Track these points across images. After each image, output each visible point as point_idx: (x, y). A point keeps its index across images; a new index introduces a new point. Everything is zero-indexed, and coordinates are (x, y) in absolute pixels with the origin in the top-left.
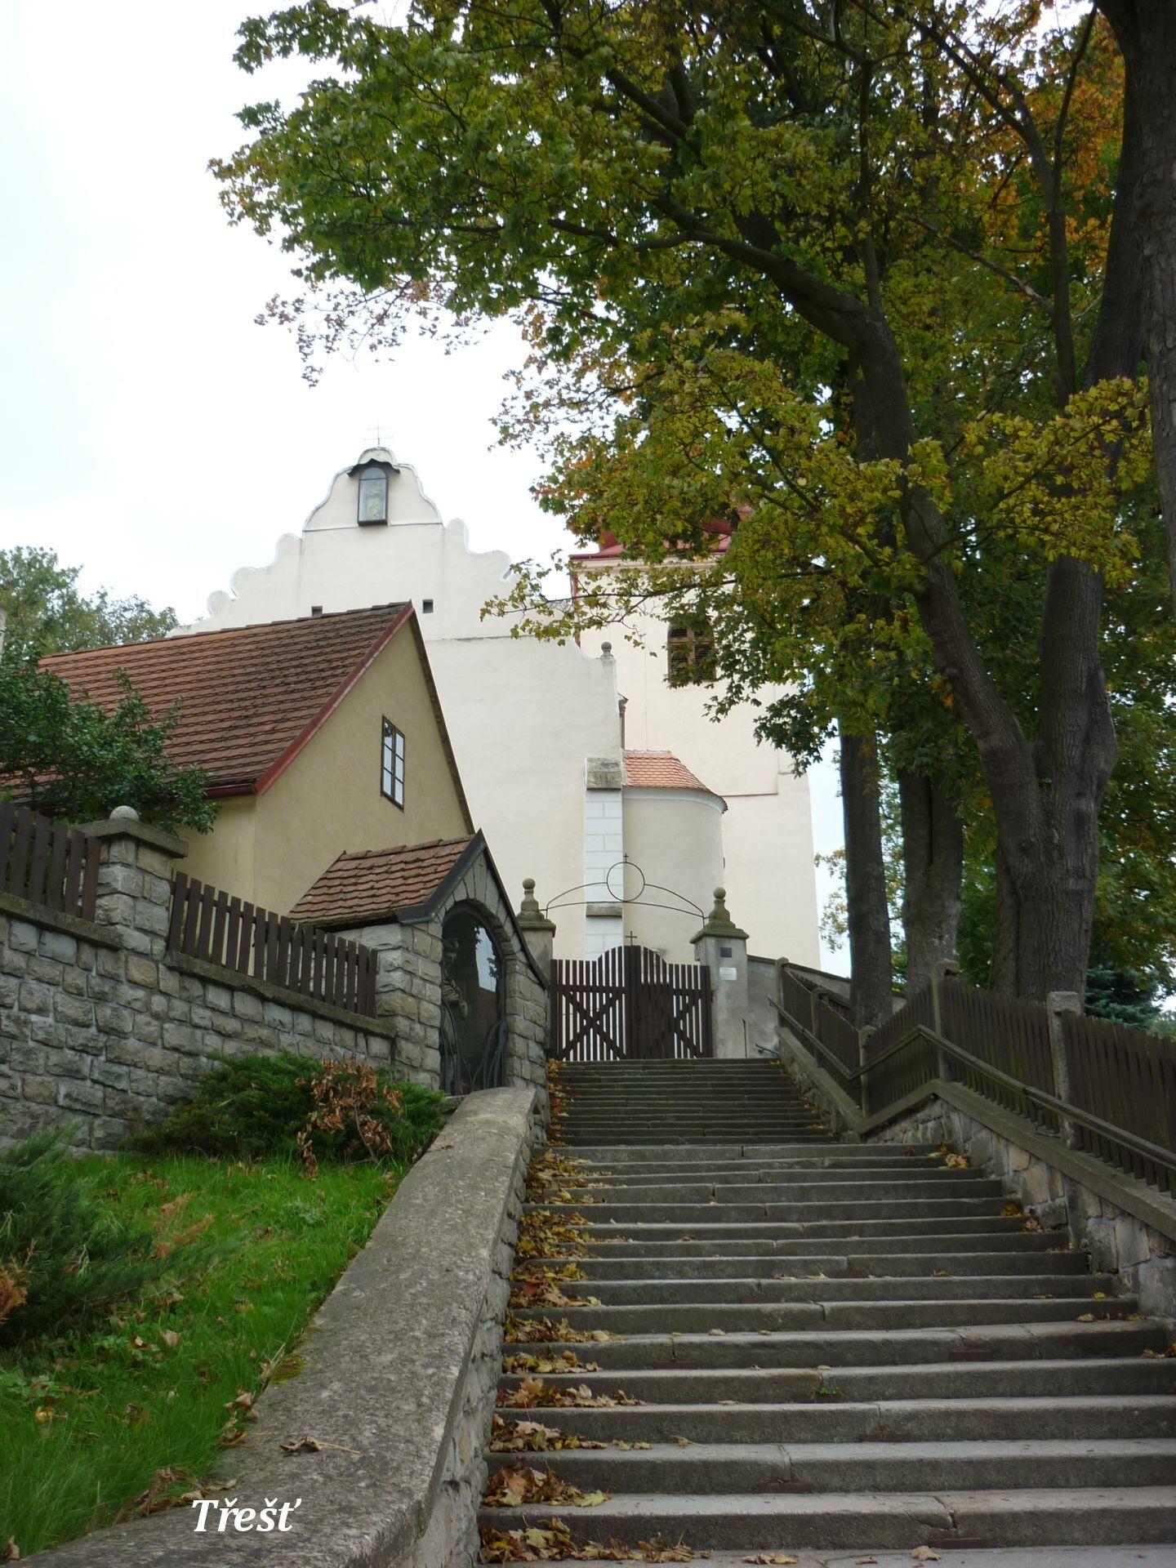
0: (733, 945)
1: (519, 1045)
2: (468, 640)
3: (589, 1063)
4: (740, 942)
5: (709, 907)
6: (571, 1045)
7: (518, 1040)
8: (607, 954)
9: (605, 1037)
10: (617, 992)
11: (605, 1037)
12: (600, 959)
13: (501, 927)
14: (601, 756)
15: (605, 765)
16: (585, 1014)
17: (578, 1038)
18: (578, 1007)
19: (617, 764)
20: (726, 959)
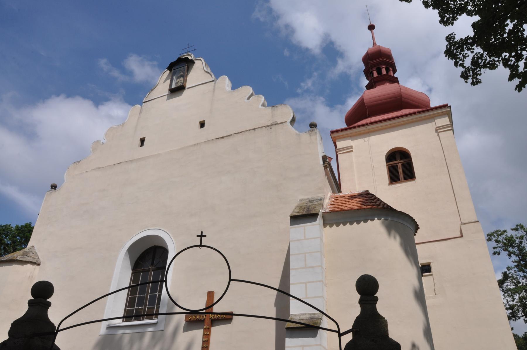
14: (310, 197)
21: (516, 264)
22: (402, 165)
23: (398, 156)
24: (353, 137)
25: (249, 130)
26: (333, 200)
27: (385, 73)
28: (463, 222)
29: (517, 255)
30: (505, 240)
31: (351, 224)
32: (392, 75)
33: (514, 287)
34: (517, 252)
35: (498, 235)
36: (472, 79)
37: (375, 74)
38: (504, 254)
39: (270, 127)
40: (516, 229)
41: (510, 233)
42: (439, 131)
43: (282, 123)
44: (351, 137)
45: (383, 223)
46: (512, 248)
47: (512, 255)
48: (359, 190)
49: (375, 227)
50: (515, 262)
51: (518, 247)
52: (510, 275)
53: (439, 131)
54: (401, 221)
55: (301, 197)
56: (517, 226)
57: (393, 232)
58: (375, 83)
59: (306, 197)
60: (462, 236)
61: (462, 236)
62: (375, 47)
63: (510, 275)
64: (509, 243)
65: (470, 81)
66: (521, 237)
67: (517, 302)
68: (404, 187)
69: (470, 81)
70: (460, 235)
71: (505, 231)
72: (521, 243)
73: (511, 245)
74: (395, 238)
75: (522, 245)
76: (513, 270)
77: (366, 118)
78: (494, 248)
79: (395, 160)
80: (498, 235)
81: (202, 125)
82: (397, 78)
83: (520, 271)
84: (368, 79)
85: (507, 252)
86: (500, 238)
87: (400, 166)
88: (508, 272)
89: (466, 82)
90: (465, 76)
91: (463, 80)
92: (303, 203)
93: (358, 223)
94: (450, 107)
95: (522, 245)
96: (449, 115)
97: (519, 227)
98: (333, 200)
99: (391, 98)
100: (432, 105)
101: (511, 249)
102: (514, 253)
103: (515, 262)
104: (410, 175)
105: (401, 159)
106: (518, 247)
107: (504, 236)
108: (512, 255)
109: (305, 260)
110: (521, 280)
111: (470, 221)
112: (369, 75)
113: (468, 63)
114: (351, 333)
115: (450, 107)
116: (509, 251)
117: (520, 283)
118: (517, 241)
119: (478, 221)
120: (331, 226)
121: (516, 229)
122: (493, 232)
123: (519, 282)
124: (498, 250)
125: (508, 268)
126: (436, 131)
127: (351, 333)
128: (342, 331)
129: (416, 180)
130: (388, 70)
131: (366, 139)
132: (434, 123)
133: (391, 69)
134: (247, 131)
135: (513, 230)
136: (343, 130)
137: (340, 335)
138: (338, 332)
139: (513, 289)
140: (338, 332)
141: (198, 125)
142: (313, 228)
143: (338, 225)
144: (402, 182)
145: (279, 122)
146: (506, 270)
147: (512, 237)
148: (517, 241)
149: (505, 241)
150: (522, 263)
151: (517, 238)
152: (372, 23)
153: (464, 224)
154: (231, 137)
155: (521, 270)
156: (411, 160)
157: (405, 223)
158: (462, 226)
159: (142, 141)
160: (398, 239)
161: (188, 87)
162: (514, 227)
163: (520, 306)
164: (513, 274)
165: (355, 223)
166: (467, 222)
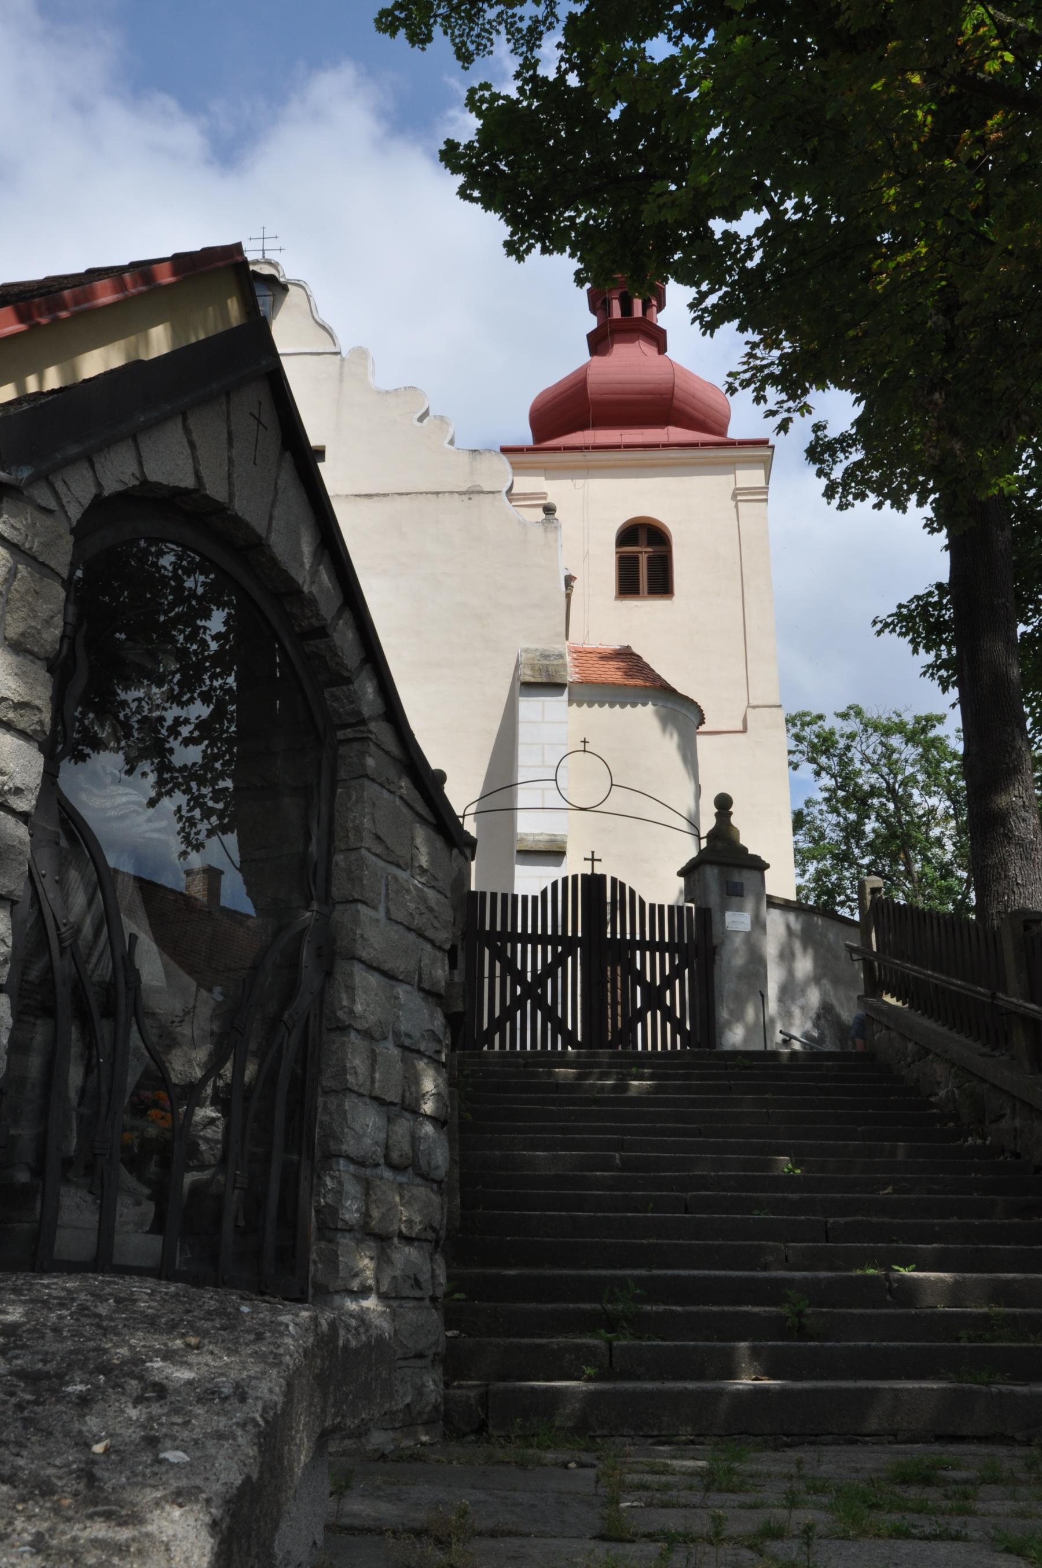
0: (746, 877)
1: (364, 998)
2: (369, 496)
3: (513, 1053)
4: (756, 874)
5: (708, 823)
6: (497, 1025)
7: (366, 981)
8: (555, 885)
9: (550, 1014)
10: (570, 944)
11: (550, 1014)
12: (544, 893)
13: (322, 632)
14: (540, 646)
15: (546, 656)
16: (519, 977)
17: (508, 1013)
18: (509, 965)
19: (561, 656)
20: (735, 900)
21: (826, 795)
22: (649, 559)
23: (643, 536)
24: (551, 472)
25: (427, 493)
26: (575, 655)
28: (753, 702)
29: (833, 776)
30: (817, 736)
31: (612, 706)
33: (811, 845)
34: (836, 769)
35: (804, 725)
36: (841, 498)
37: (617, 313)
38: (807, 769)
40: (844, 716)
41: (831, 723)
42: (739, 498)
43: (493, 493)
44: (545, 469)
45: (657, 713)
46: (828, 758)
47: (823, 774)
48: (615, 643)
49: (644, 716)
50: (827, 790)
51: (840, 756)
52: (808, 818)
53: (739, 498)
54: (684, 711)
55: (525, 645)
56: (850, 708)
57: (670, 727)
59: (533, 646)
60: (745, 730)
61: (745, 730)
63: (808, 818)
64: (824, 744)
65: (836, 502)
66: (852, 736)
67: (808, 881)
68: (646, 610)
69: (836, 502)
70: (740, 728)
71: (821, 717)
72: (848, 748)
73: (826, 752)
74: (671, 735)
75: (849, 755)
76: (818, 807)
77: (583, 426)
78: (790, 752)
79: (635, 543)
80: (803, 725)
83: (831, 812)
85: (815, 766)
86: (807, 732)
87: (645, 560)
88: (805, 812)
89: (829, 503)
90: (829, 493)
91: (825, 500)
92: (533, 659)
93: (623, 705)
94: (773, 447)
95: (849, 755)
96: (767, 464)
97: (852, 712)
99: (650, 393)
100: (734, 432)
101: (823, 760)
102: (827, 769)
103: (827, 790)
104: (662, 584)
105: (649, 544)
106: (840, 756)
107: (815, 728)
108: (823, 774)
109: (543, 754)
110: (829, 833)
111: (766, 704)
112: (599, 304)
113: (837, 474)
115: (773, 447)
116: (818, 764)
117: (825, 838)
118: (842, 743)
119: (780, 706)
120: (580, 705)
121: (844, 716)
122: (793, 714)
123: (822, 836)
124: (795, 758)
125: (809, 803)
126: (734, 496)
129: (674, 598)
131: (580, 482)
132: (732, 476)
133: (654, 302)
134: (421, 493)
135: (838, 715)
136: (530, 450)
139: (809, 850)
142: (556, 705)
143: (590, 705)
144: (644, 598)
145: (486, 489)
146: (803, 806)
147: (832, 733)
148: (842, 743)
149: (816, 741)
150: (841, 794)
151: (842, 736)
153: (754, 707)
155: (835, 810)
156: (670, 551)
157: (689, 715)
158: (750, 711)
160: (676, 737)
162: (843, 709)
163: (814, 889)
164: (814, 818)
165: (618, 706)
166: (760, 704)
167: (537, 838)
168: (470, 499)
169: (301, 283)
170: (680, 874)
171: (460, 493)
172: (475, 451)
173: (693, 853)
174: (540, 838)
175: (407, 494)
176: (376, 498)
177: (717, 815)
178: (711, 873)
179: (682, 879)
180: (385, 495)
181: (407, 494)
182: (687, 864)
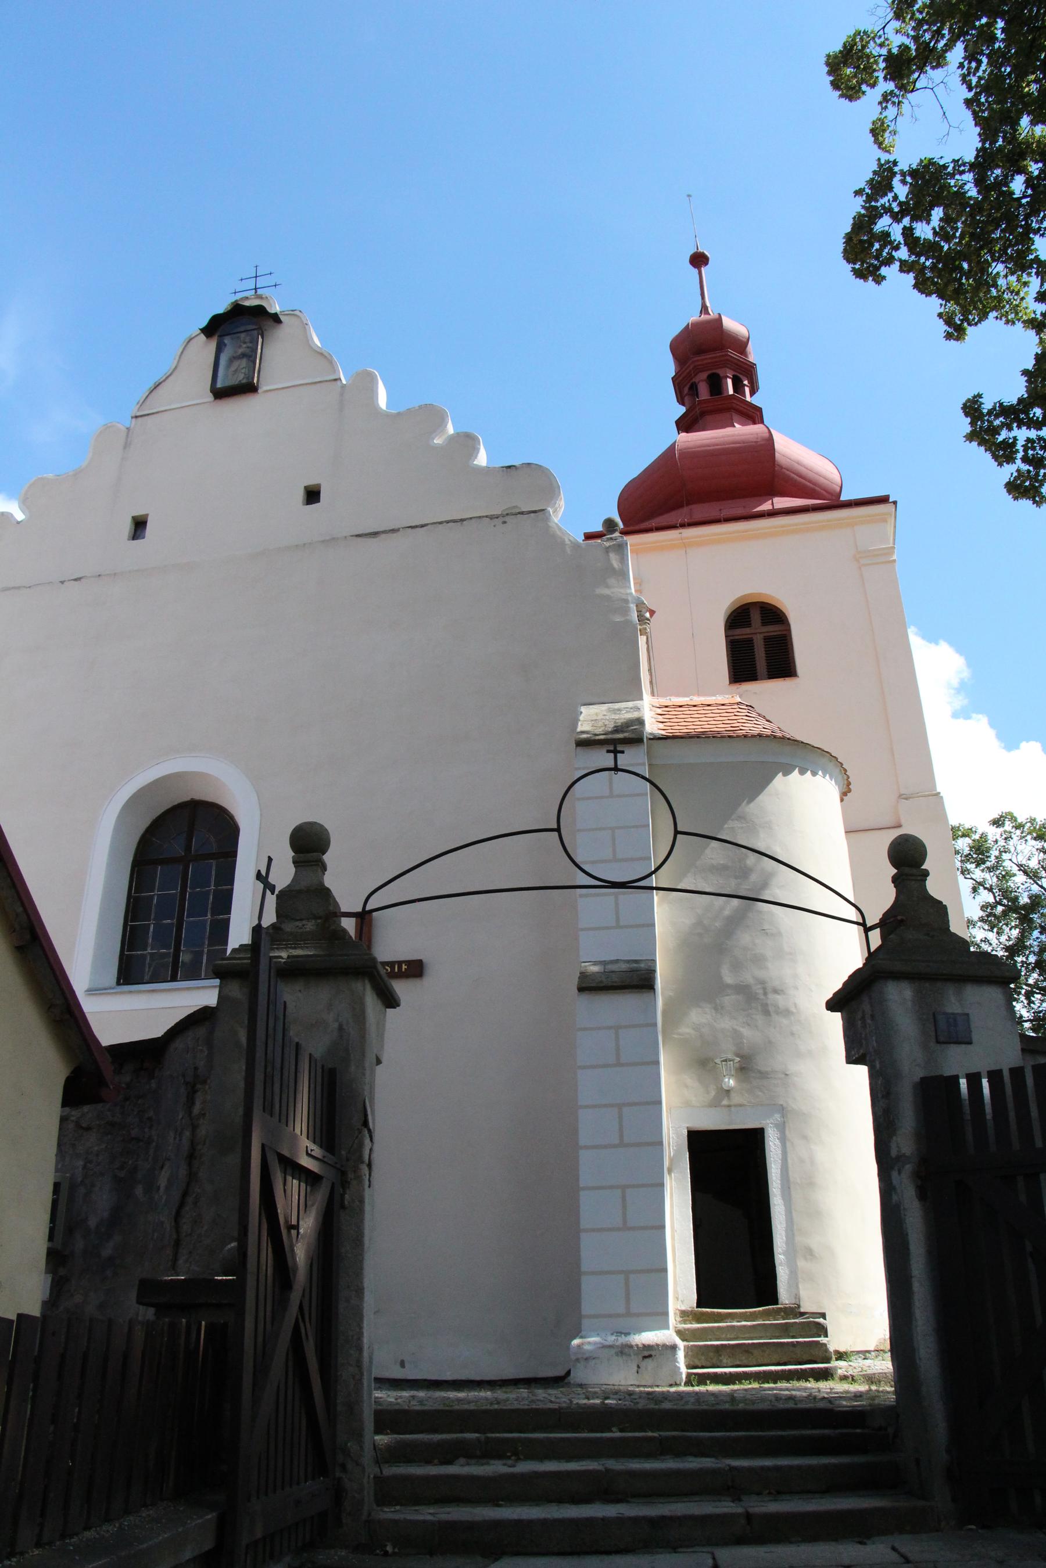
2: (375, 534)
23: (756, 617)
25: (448, 522)
26: (659, 711)
27: (731, 392)
29: (990, 890)
32: (748, 398)
39: (501, 519)
41: (984, 827)
58: (703, 414)
62: (704, 317)
68: (766, 693)
81: (312, 495)
82: (759, 410)
84: (681, 401)
92: (597, 714)
94: (895, 503)
98: (659, 711)
104: (781, 664)
112: (686, 390)
114: (878, 930)
115: (895, 503)
127: (878, 930)
128: (869, 924)
130: (738, 386)
137: (867, 930)
138: (863, 924)
140: (863, 924)
141: (300, 495)
152: (700, 250)
154: (399, 534)
159: (139, 525)
161: (265, 388)
167: (610, 967)
168: (504, 522)
169: (297, 313)
170: (833, 1005)
171: (491, 517)
172: (509, 467)
173: (855, 961)
174: (614, 967)
175: (422, 526)
176: (383, 536)
177: (895, 880)
178: (899, 997)
179: (837, 1018)
180: (393, 531)
181: (422, 526)
182: (845, 984)
